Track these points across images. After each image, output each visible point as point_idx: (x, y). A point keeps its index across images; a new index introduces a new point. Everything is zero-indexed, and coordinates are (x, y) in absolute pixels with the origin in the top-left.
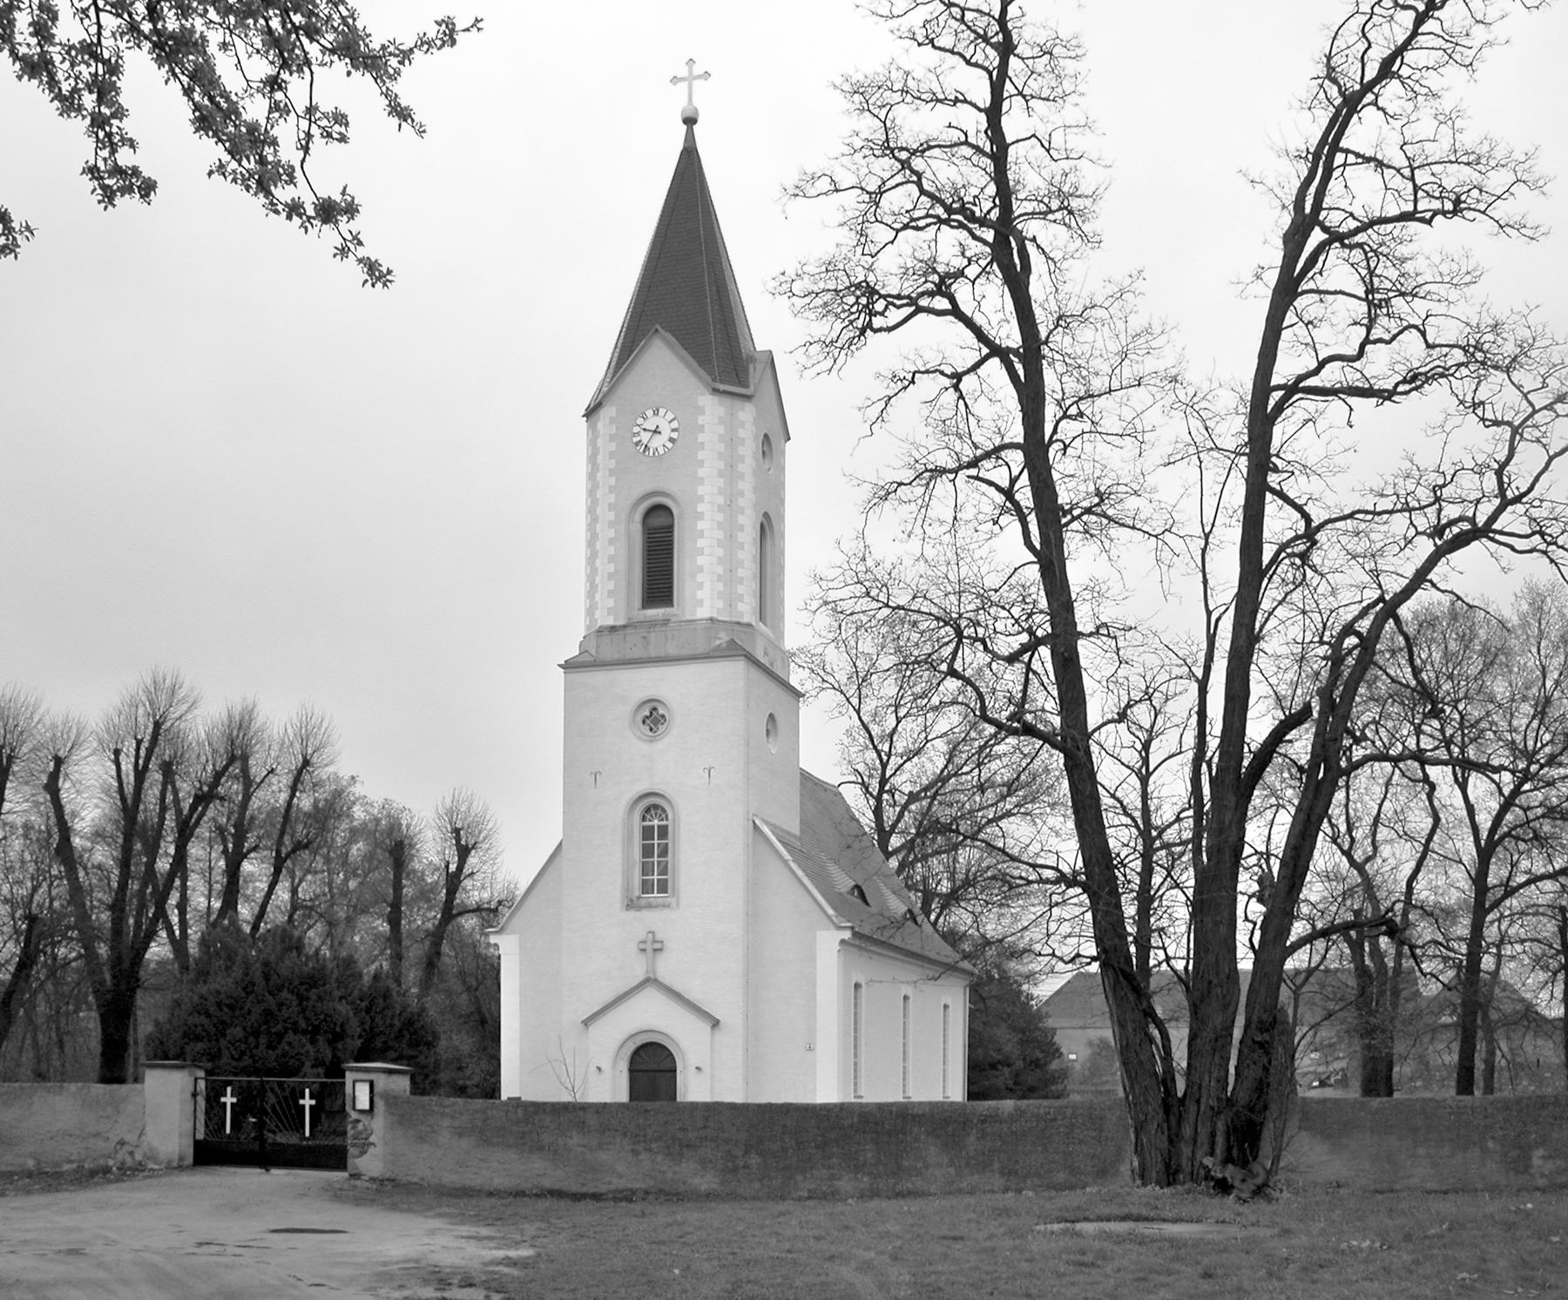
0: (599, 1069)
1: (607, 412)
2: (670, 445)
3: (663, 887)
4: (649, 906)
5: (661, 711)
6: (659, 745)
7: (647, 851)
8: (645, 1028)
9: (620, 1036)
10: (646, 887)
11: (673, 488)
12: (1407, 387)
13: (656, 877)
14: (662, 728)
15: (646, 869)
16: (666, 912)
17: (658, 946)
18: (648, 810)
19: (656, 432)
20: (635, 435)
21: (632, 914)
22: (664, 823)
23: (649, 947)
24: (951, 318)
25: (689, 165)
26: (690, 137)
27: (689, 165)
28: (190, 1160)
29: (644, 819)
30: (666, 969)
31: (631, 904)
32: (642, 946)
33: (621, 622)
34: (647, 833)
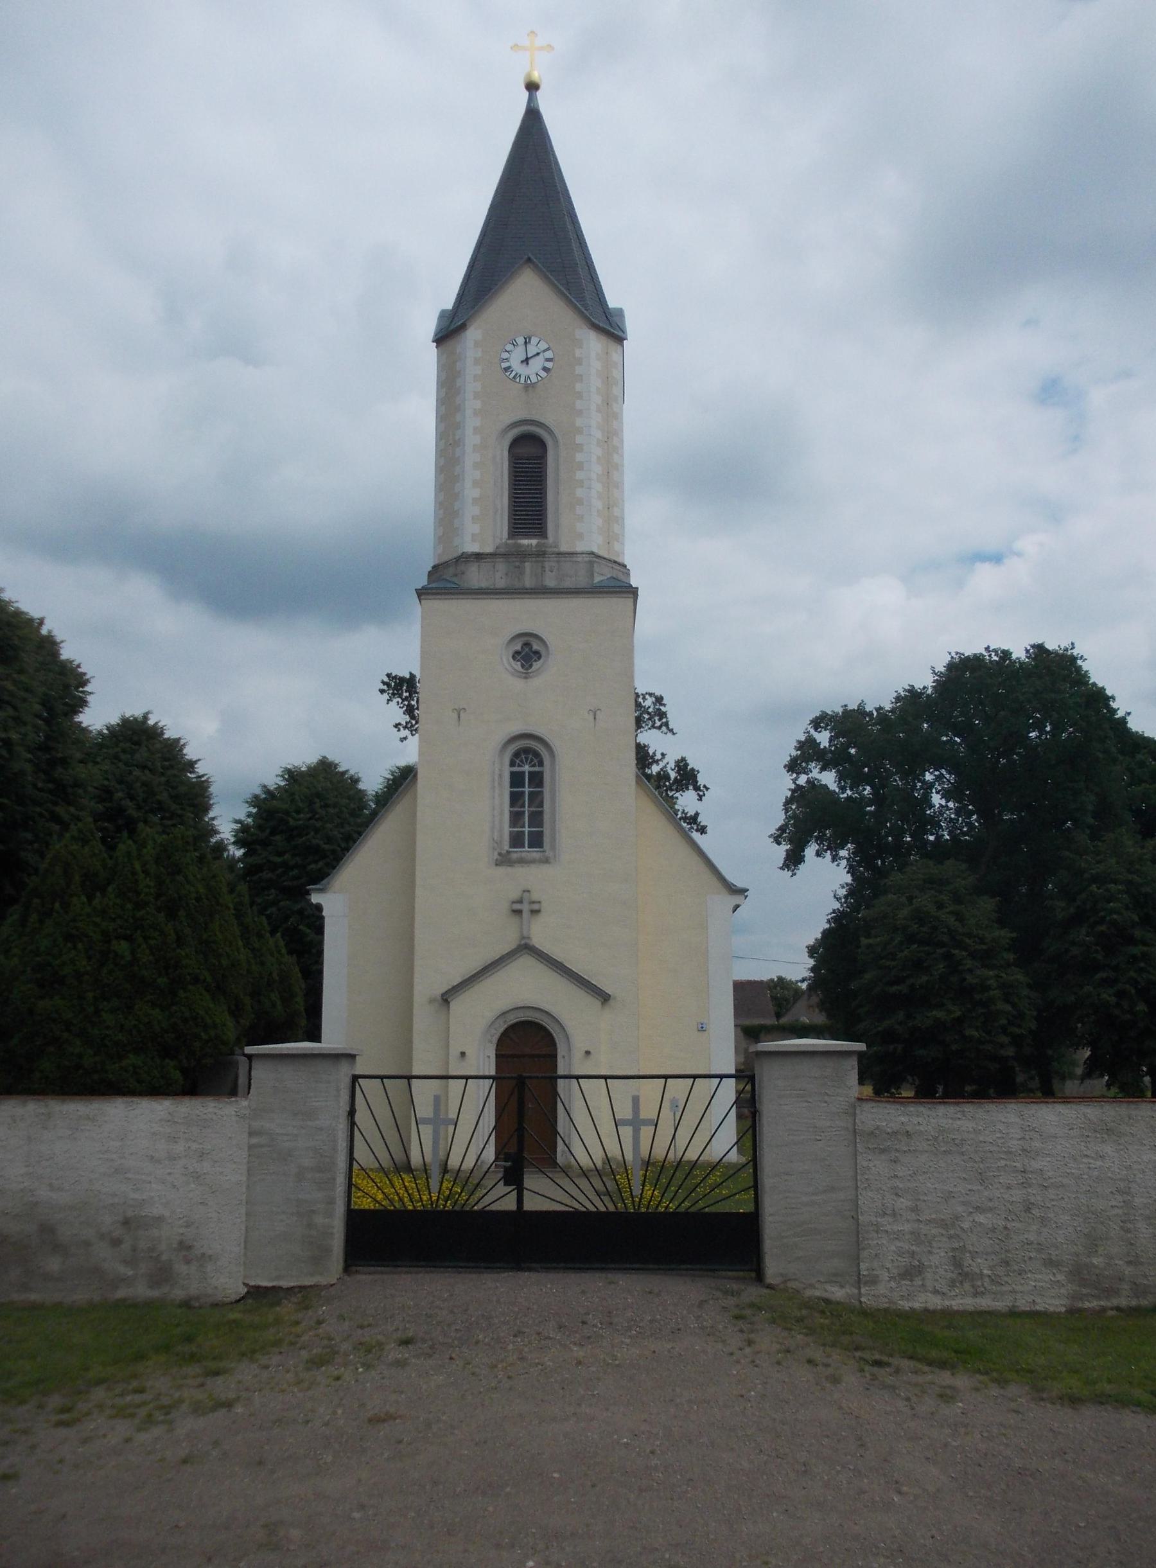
0: (463, 1054)
1: (473, 334)
2: (543, 374)
3: (537, 841)
4: (522, 861)
5: (535, 647)
6: (536, 682)
7: (515, 798)
8: (521, 1004)
9: (490, 1014)
10: (516, 841)
11: (549, 419)
12: (499, 576)
13: (527, 829)
14: (536, 665)
15: (516, 818)
16: (545, 868)
17: (535, 907)
18: (517, 755)
19: (526, 361)
20: (503, 360)
21: (502, 870)
22: (537, 769)
23: (525, 907)
24: (525, 357)
25: (532, 124)
26: (531, 99)
27: (532, 124)
28: (357, 1057)
29: (512, 764)
30: (541, 934)
31: (504, 860)
32: (517, 907)
33: (489, 549)
34: (516, 779)
